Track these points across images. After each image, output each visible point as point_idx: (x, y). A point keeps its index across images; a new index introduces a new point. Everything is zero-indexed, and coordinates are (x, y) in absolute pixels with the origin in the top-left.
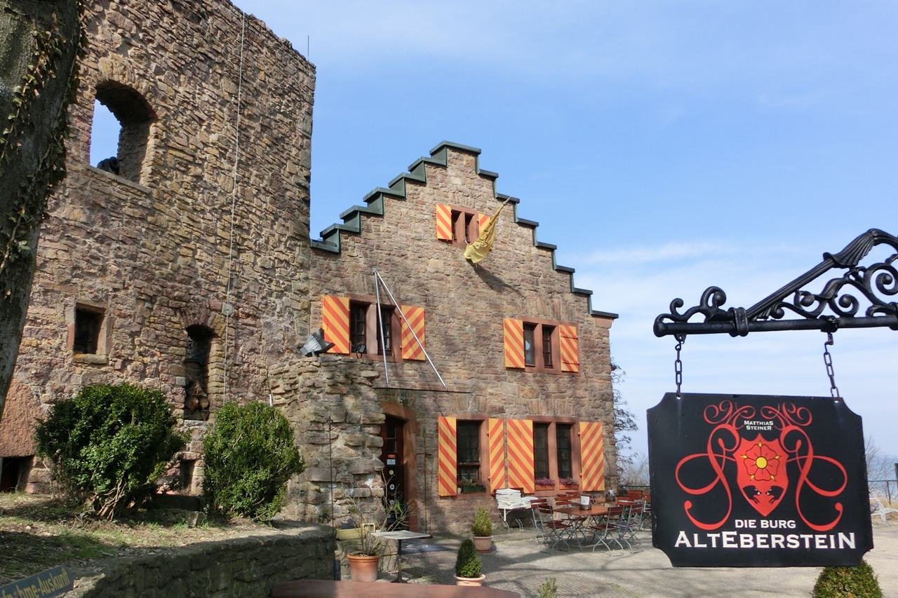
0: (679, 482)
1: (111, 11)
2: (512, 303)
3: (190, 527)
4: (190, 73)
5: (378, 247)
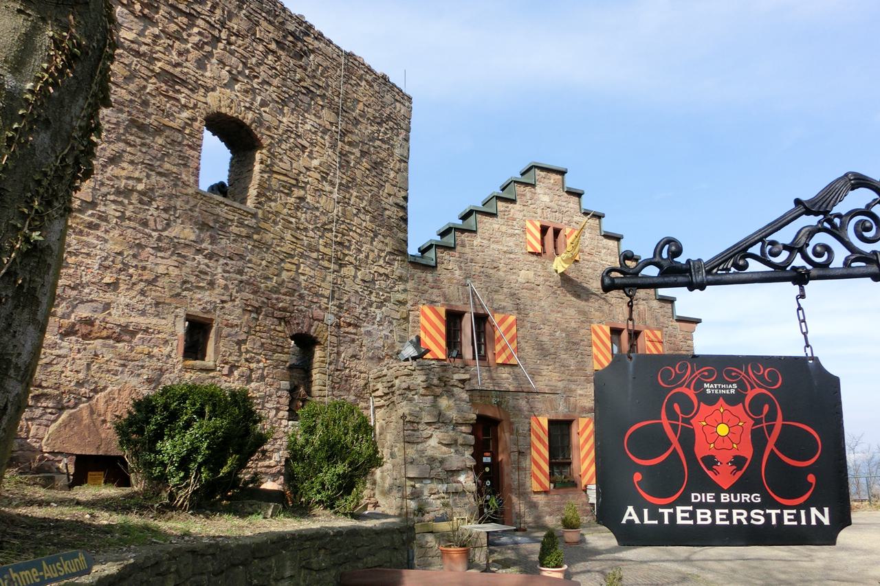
0: (627, 450)
1: (219, 51)
2: (600, 309)
3: (265, 518)
4: (293, 105)
5: (472, 261)
